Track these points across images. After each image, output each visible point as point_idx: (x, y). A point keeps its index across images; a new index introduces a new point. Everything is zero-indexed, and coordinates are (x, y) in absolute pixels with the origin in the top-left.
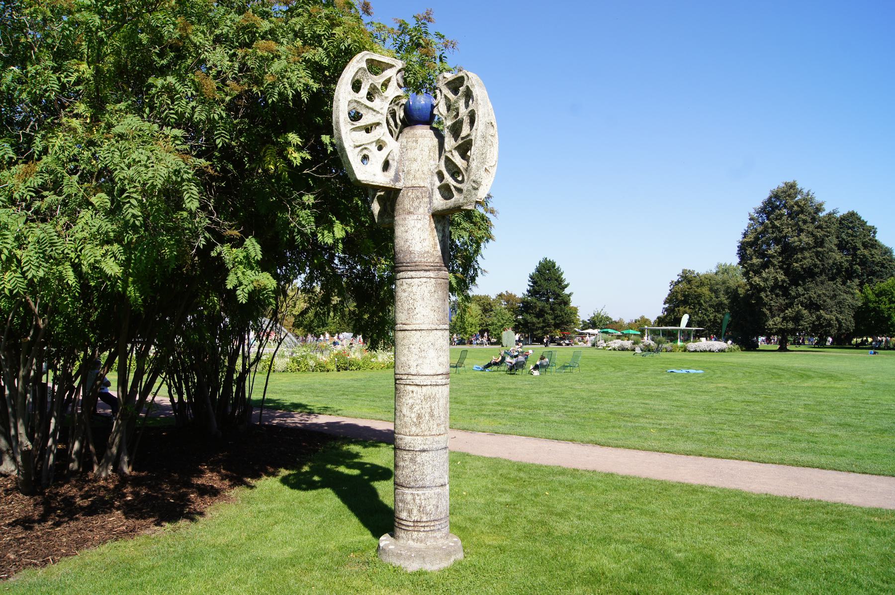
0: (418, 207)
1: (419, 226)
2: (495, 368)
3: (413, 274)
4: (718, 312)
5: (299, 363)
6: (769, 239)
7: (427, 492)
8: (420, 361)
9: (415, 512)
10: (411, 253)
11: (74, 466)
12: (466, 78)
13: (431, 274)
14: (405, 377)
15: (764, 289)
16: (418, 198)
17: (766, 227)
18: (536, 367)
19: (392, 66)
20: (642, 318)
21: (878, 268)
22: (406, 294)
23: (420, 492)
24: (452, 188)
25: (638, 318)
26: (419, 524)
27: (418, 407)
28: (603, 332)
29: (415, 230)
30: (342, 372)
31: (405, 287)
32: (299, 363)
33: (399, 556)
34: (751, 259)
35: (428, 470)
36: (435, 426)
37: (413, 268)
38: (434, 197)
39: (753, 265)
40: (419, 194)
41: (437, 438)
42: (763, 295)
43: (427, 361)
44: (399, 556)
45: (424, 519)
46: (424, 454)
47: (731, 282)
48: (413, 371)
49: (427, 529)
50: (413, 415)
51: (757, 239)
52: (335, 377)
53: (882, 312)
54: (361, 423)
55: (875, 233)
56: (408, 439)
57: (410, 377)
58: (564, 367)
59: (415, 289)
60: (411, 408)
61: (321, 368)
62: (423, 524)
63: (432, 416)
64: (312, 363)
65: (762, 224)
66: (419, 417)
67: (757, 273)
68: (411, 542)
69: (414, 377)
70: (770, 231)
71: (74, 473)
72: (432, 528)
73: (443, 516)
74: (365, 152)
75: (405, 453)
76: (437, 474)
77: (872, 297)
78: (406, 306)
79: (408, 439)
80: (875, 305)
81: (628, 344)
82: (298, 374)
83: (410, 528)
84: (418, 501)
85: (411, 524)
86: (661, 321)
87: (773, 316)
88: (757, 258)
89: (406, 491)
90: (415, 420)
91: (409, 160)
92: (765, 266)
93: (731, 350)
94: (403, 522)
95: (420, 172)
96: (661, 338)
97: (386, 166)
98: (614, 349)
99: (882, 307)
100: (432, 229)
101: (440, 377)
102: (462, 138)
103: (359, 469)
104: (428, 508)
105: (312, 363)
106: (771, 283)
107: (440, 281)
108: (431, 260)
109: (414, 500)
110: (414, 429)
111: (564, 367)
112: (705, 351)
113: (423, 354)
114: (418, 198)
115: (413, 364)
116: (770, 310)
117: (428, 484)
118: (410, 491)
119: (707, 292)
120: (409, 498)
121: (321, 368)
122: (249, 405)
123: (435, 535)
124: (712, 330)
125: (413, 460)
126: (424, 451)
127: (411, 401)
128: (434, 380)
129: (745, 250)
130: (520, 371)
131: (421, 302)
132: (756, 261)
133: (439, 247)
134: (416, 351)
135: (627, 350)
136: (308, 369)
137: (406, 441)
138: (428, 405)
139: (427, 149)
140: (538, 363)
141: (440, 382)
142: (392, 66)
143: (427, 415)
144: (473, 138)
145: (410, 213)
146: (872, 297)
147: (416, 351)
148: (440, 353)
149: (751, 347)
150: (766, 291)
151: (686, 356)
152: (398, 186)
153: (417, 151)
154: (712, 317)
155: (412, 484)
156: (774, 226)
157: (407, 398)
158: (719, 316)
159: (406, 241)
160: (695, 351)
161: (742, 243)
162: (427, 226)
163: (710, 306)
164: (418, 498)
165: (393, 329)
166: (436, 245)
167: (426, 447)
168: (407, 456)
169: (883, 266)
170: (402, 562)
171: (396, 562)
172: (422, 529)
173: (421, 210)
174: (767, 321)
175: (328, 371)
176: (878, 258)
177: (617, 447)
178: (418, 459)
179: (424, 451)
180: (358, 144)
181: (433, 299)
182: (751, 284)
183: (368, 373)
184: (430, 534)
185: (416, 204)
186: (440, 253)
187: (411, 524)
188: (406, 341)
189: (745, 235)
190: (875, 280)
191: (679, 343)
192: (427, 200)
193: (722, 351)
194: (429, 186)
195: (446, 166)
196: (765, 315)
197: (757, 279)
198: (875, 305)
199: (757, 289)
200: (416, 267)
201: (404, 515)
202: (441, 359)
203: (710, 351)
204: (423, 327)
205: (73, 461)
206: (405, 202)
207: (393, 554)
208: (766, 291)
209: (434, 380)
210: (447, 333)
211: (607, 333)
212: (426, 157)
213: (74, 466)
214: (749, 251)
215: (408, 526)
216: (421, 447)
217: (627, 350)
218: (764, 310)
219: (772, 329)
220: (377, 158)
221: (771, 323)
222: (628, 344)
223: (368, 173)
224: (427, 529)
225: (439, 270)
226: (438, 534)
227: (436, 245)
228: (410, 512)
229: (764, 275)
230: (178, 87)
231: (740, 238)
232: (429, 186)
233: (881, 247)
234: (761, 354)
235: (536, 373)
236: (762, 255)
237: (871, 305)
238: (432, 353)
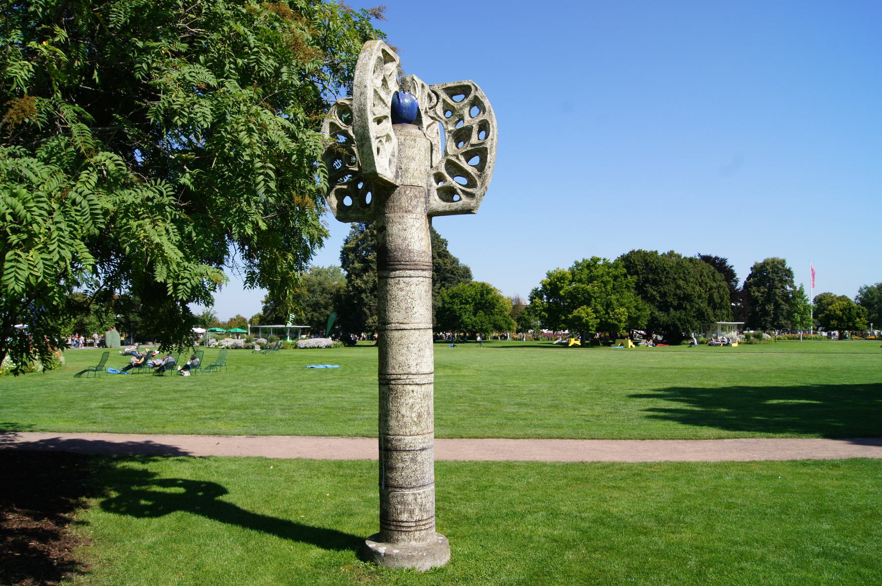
0: (416, 207)
1: (417, 225)
2: (136, 370)
3: (411, 273)
4: (314, 310)
6: (368, 246)
8: (419, 361)
9: (417, 511)
10: (410, 252)
12: (473, 88)
14: (402, 377)
15: (364, 291)
16: (416, 197)
17: (366, 235)
18: (186, 368)
20: (238, 316)
21: (449, 275)
22: (404, 293)
23: (421, 491)
24: (459, 191)
25: (234, 316)
26: (421, 523)
27: (418, 406)
28: (212, 331)
29: (414, 228)
31: (402, 285)
33: (410, 558)
34: (353, 263)
37: (413, 267)
38: (431, 198)
39: (355, 268)
40: (417, 193)
42: (363, 296)
43: (425, 360)
44: (410, 558)
45: (425, 517)
46: (424, 452)
47: (326, 283)
48: (413, 370)
49: (427, 526)
50: (413, 415)
51: (357, 245)
53: (455, 311)
54: (65, 437)
55: (446, 245)
56: (408, 439)
57: (411, 376)
58: (212, 366)
59: (413, 288)
60: (412, 407)
62: (424, 523)
65: (362, 232)
66: (419, 416)
67: (358, 276)
68: (413, 543)
69: (415, 376)
70: (370, 238)
75: (405, 453)
77: (447, 299)
78: (403, 305)
79: (408, 439)
80: (450, 305)
81: (241, 342)
83: (413, 529)
84: (419, 500)
86: (263, 320)
87: (372, 315)
88: (359, 262)
89: (406, 492)
90: (415, 419)
91: (408, 158)
92: (365, 270)
93: (336, 346)
94: (403, 524)
95: (418, 172)
96: (272, 336)
98: (228, 348)
99: (455, 307)
102: (472, 145)
103: (185, 487)
106: (370, 285)
109: (416, 499)
110: (414, 428)
111: (212, 366)
112: (314, 348)
113: (422, 353)
114: (416, 197)
115: (413, 363)
116: (369, 309)
118: (412, 491)
119: (306, 293)
120: (410, 498)
124: (317, 330)
125: (413, 460)
126: (423, 449)
127: (411, 401)
129: (347, 255)
130: (167, 372)
131: (419, 301)
132: (357, 265)
134: (415, 350)
135: (241, 348)
137: (406, 441)
140: (189, 363)
144: (488, 146)
145: (410, 211)
146: (447, 299)
147: (415, 350)
149: (351, 344)
150: (366, 293)
151: (297, 353)
152: (398, 182)
153: (416, 150)
154: (309, 315)
155: (414, 484)
156: (372, 235)
157: (407, 398)
158: (316, 314)
159: (405, 239)
160: (305, 348)
161: (345, 249)
163: (308, 306)
164: (419, 497)
167: (425, 445)
168: (407, 457)
169: (452, 273)
170: (414, 563)
171: (407, 565)
172: (423, 527)
173: (419, 209)
174: (367, 319)
176: (449, 267)
178: (419, 459)
179: (423, 449)
182: (353, 286)
185: (414, 203)
188: (404, 340)
189: (347, 242)
190: (447, 285)
191: (289, 340)
192: (423, 200)
193: (328, 347)
194: (425, 185)
195: (447, 169)
196: (365, 313)
197: (359, 281)
198: (450, 305)
199: (359, 291)
200: (415, 267)
201: (404, 517)
203: (318, 347)
204: (421, 326)
206: (402, 199)
207: (403, 558)
208: (366, 293)
210: (431, 331)
211: (215, 331)
212: (422, 158)
214: (351, 256)
215: (410, 527)
216: (421, 446)
217: (241, 348)
218: (365, 309)
219: (371, 327)
221: (370, 321)
222: (241, 342)
223: (384, 168)
224: (427, 526)
228: (411, 512)
229: (365, 278)
231: (342, 244)
232: (425, 185)
233: (451, 257)
234: (362, 349)
235: (187, 374)
236: (363, 260)
237: (446, 305)
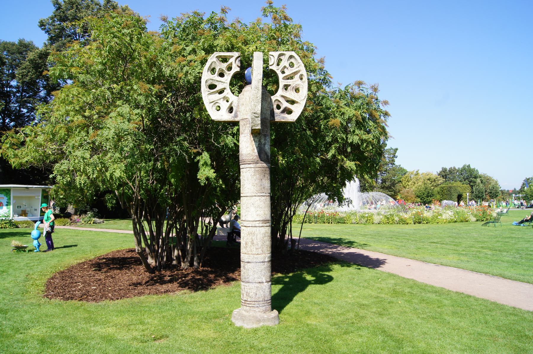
1: (245, 140)
5: (388, 218)
7: (251, 285)
11: (174, 262)
13: (252, 166)
19: (232, 56)
23: (247, 285)
30: (417, 225)
32: (388, 218)
35: (251, 273)
36: (255, 249)
41: (256, 256)
45: (249, 300)
52: (411, 228)
61: (403, 222)
63: (253, 243)
64: (396, 219)
71: (175, 266)
72: (253, 305)
73: (261, 300)
74: (217, 104)
76: (256, 276)
82: (388, 225)
84: (246, 290)
85: (243, 302)
89: (242, 283)
97: (231, 110)
100: (252, 141)
101: (258, 222)
104: (251, 294)
105: (396, 219)
107: (257, 169)
108: (251, 158)
113: (248, 209)
114: (244, 125)
117: (250, 281)
120: (243, 287)
121: (403, 222)
122: (293, 241)
123: (255, 309)
126: (249, 262)
128: (254, 224)
133: (256, 151)
136: (394, 223)
138: (250, 237)
139: (248, 98)
141: (257, 225)
142: (232, 56)
143: (250, 243)
148: (258, 209)
152: (236, 119)
153: (244, 100)
162: (249, 140)
165: (271, 196)
166: (254, 149)
167: (249, 260)
173: (246, 131)
175: (407, 224)
177: (516, 280)
179: (249, 262)
180: (211, 101)
181: (253, 179)
183: (435, 225)
184: (252, 309)
186: (257, 154)
187: (243, 302)
202: (258, 212)
205: (174, 260)
209: (254, 224)
213: (174, 262)
220: (225, 106)
225: (256, 163)
226: (257, 310)
227: (254, 149)
230: (153, 88)
238: (252, 209)
